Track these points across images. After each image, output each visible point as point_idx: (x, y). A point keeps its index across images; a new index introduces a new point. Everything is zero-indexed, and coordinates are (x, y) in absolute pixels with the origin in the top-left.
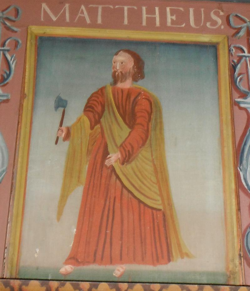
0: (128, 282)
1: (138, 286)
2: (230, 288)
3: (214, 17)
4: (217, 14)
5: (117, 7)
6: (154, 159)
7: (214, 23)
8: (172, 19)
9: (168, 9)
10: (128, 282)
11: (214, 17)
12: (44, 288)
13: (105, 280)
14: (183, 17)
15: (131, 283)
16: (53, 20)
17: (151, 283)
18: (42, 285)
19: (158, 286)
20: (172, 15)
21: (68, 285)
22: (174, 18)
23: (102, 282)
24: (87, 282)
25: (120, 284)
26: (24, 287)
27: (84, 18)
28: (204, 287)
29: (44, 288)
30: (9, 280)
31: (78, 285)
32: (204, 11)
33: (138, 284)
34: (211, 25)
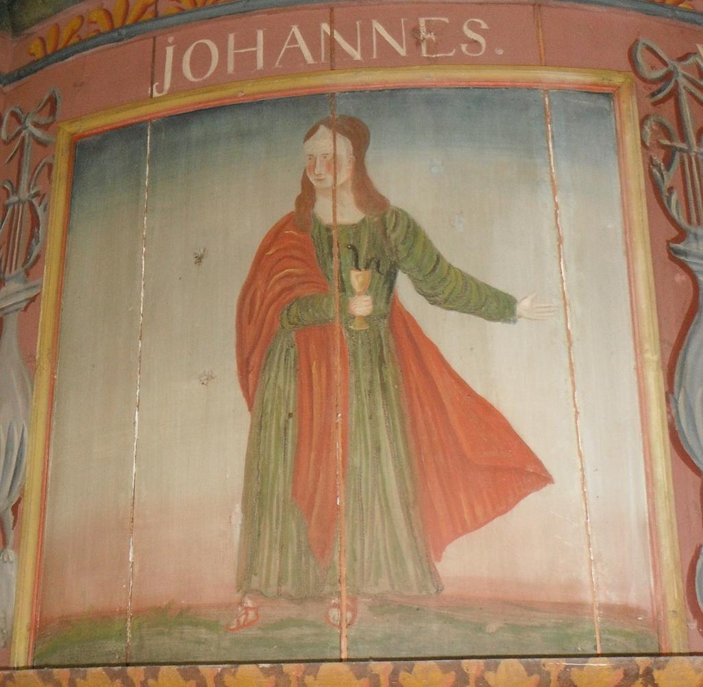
18: (445, 670)
27: (299, 50)
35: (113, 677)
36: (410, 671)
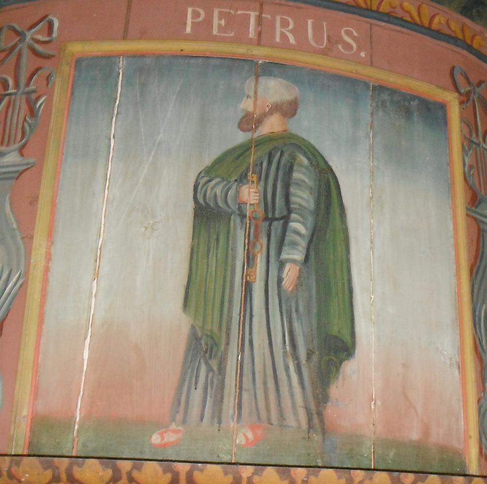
0: (255, 465)
1: (270, 473)
2: (41, 463)
5: (239, 12)
6: (14, 231)
7: (348, 46)
8: (220, 25)
10: (255, 465)
13: (435, 471)
14: (237, 24)
15: (76, 459)
16: (212, 32)
17: (403, 471)
19: (411, 477)
20: (220, 19)
21: (270, 473)
22: (223, 22)
23: (432, 473)
24: (188, 464)
26: (256, 479)
28: (143, 464)
29: (286, 482)
30: (52, 458)
32: (327, 25)
33: (269, 468)
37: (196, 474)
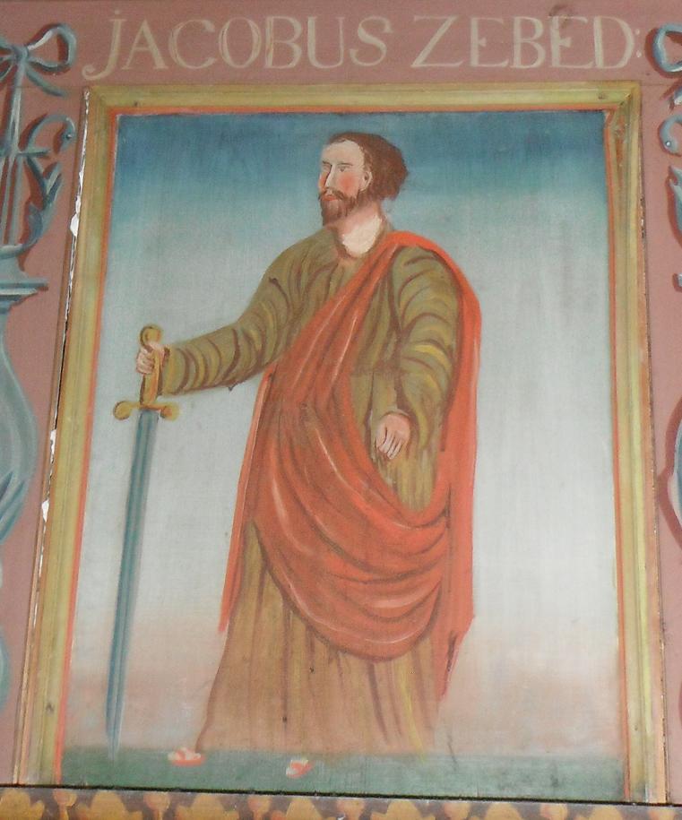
3: (363, 34)
4: (374, 29)
7: (368, 52)
9: (474, 22)
11: (363, 34)
12: (40, 807)
13: (429, 794)
25: (445, 802)
28: (488, 807)
31: (441, 807)
34: (360, 56)
35: (228, 808)
36: (189, 803)
37: (181, 809)
